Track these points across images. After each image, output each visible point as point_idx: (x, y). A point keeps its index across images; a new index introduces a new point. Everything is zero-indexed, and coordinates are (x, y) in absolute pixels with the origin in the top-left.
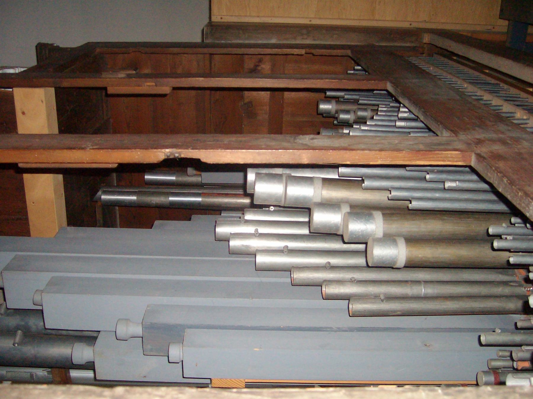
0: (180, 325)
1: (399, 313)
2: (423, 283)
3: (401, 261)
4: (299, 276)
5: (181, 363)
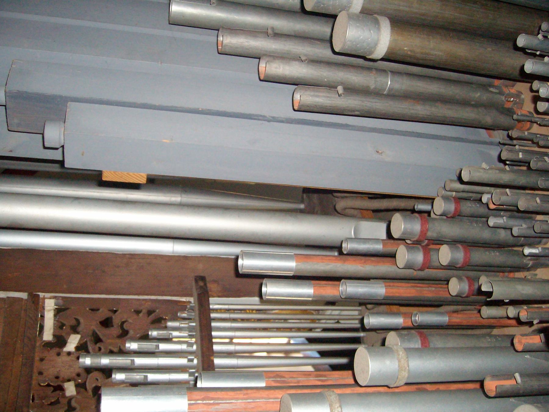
0: (61, 97)
1: (357, 113)
2: (389, 73)
3: (381, 51)
4: (230, 41)
5: (61, 149)
